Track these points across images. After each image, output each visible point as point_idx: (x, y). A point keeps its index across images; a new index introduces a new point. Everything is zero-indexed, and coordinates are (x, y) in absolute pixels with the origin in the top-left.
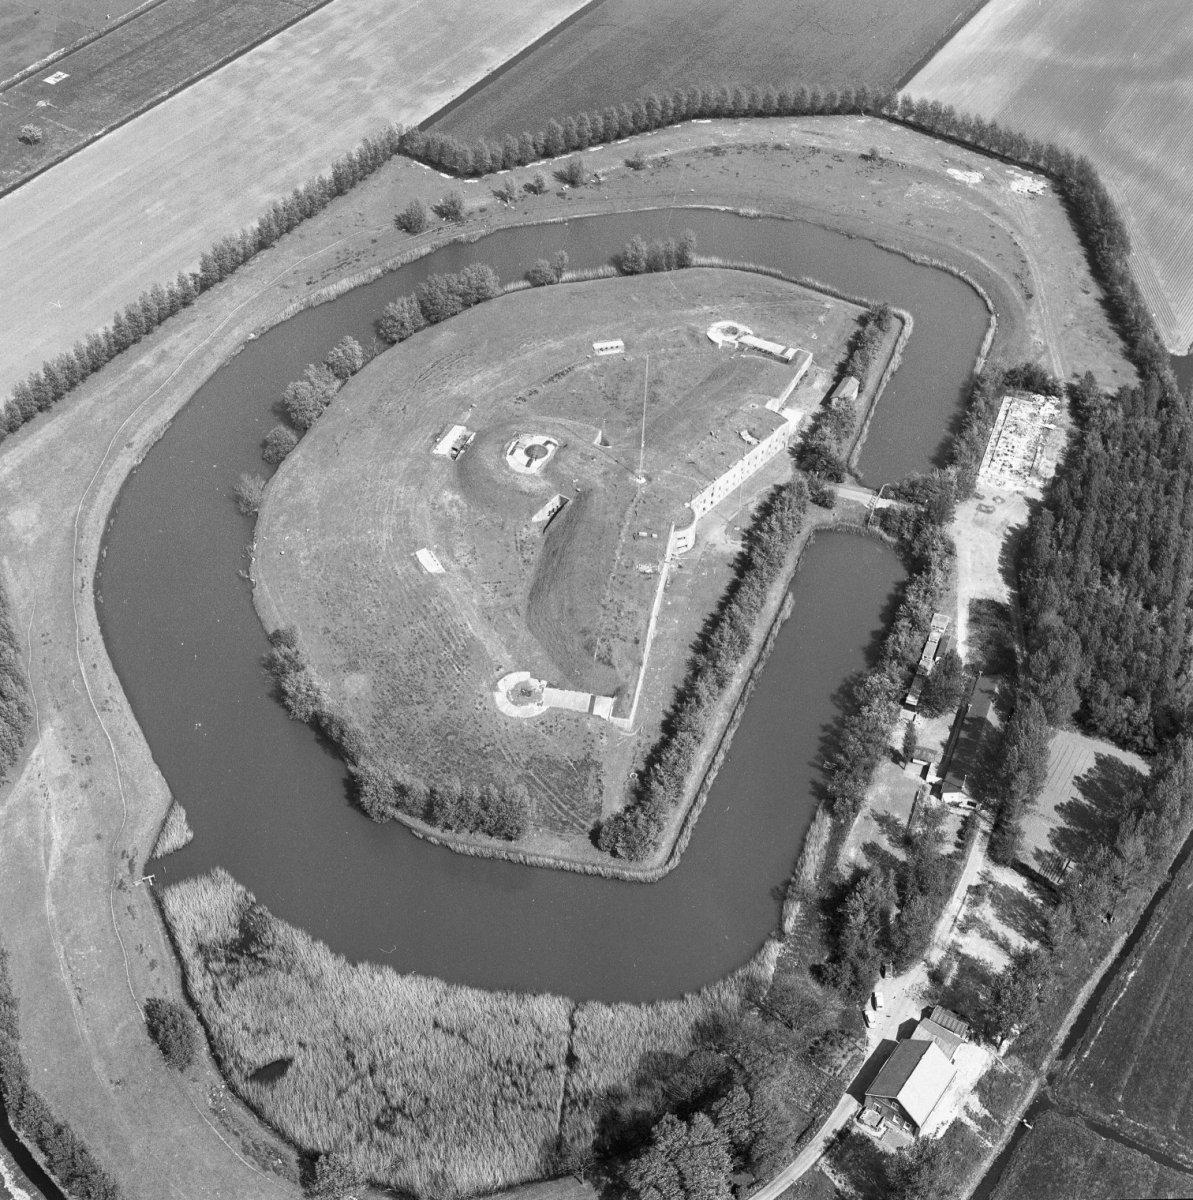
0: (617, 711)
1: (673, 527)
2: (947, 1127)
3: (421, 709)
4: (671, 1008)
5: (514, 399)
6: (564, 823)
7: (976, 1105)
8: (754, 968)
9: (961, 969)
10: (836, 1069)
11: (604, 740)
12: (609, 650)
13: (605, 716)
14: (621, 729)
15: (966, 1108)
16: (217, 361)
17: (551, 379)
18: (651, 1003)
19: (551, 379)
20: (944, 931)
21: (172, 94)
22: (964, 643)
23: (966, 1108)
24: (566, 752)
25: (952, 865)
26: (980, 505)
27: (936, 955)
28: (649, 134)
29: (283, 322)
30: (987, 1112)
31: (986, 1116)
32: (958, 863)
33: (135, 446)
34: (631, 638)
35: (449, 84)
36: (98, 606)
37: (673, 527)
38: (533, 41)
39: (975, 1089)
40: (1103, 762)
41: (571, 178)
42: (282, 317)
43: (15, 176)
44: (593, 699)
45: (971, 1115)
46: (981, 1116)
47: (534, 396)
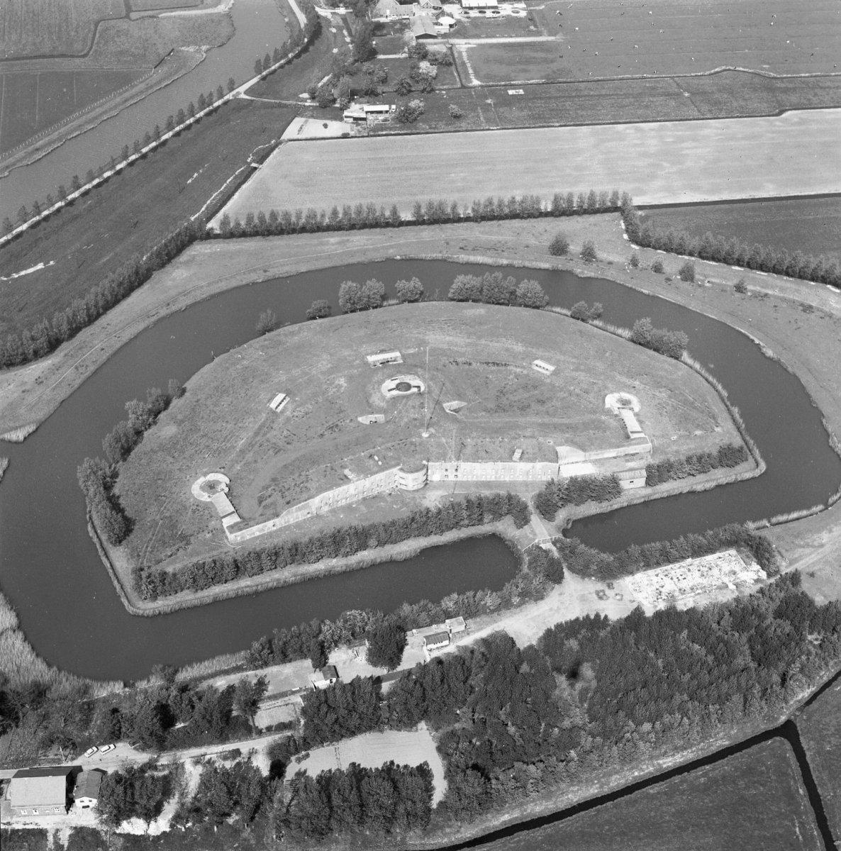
0: (233, 528)
1: (399, 467)
2: (36, 827)
3: (171, 460)
4: (41, 666)
5: (452, 360)
6: (139, 556)
7: (64, 839)
8: (96, 685)
9: (165, 777)
10: (45, 756)
11: (208, 536)
12: (270, 496)
13: (225, 526)
14: (227, 538)
15: (57, 830)
16: (363, 259)
17: (487, 363)
18: (37, 655)
19: (487, 363)
20: (186, 757)
21: (561, 126)
22: (458, 647)
23: (57, 830)
24: (184, 527)
25: (250, 731)
26: (603, 591)
27: (165, 759)
28: (776, 276)
29: (422, 260)
30: (66, 844)
31: (63, 846)
32: (254, 734)
33: (268, 274)
34: (288, 499)
35: (712, 191)
36: (146, 330)
37: (399, 467)
38: (803, 194)
39: (75, 828)
40: (423, 772)
41: (687, 275)
42: (423, 256)
43: (423, 129)
44: (233, 512)
45: (55, 836)
46: (61, 842)
47: (467, 367)
